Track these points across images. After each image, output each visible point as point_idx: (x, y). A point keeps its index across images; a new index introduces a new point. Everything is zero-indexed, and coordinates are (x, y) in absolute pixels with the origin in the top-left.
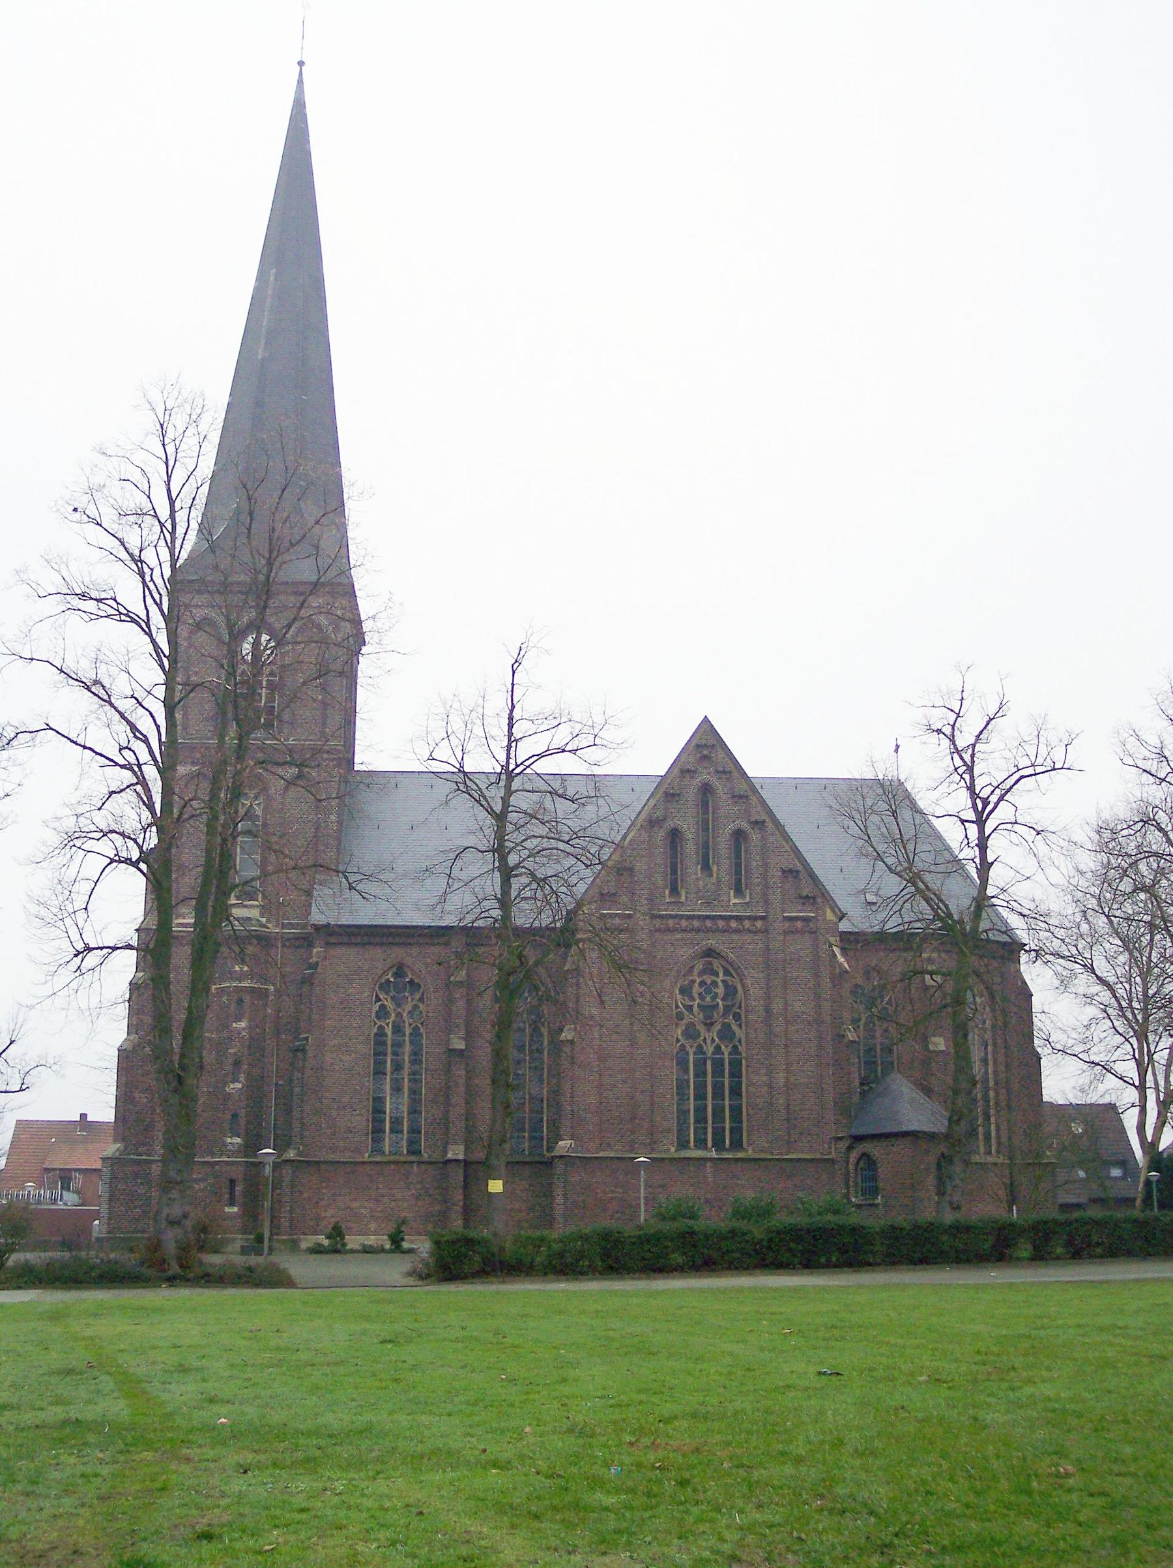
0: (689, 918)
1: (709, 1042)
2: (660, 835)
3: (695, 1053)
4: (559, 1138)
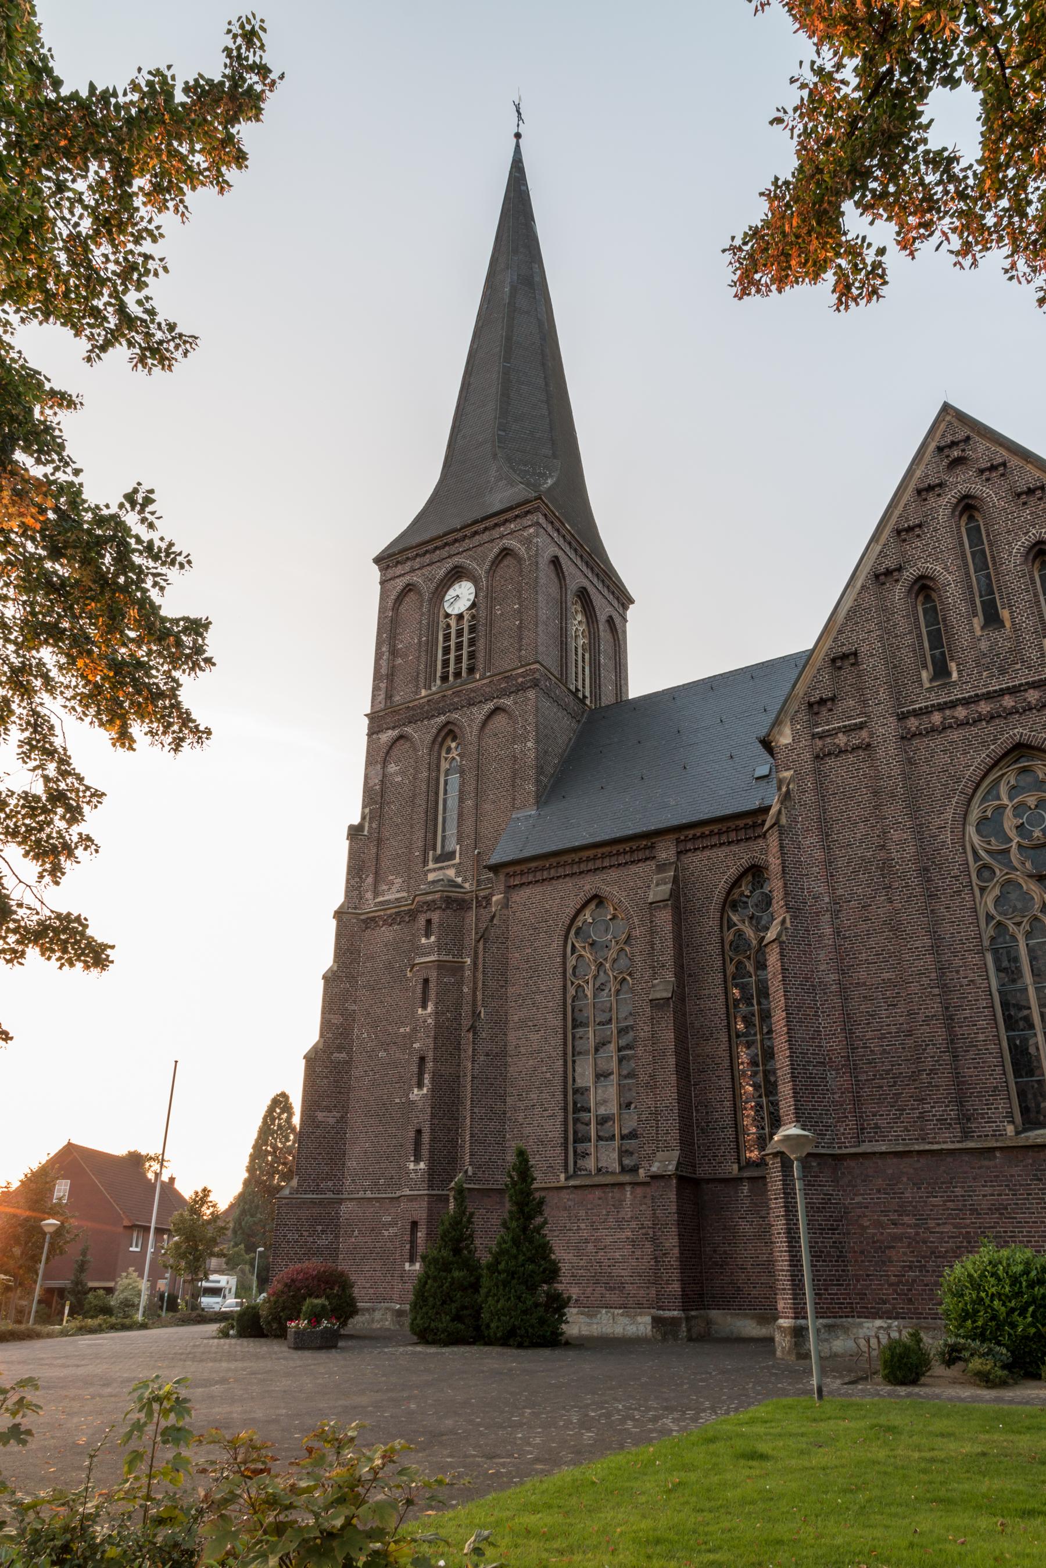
0: (966, 702)
2: (898, 592)
3: (1028, 935)
4: (776, 1123)
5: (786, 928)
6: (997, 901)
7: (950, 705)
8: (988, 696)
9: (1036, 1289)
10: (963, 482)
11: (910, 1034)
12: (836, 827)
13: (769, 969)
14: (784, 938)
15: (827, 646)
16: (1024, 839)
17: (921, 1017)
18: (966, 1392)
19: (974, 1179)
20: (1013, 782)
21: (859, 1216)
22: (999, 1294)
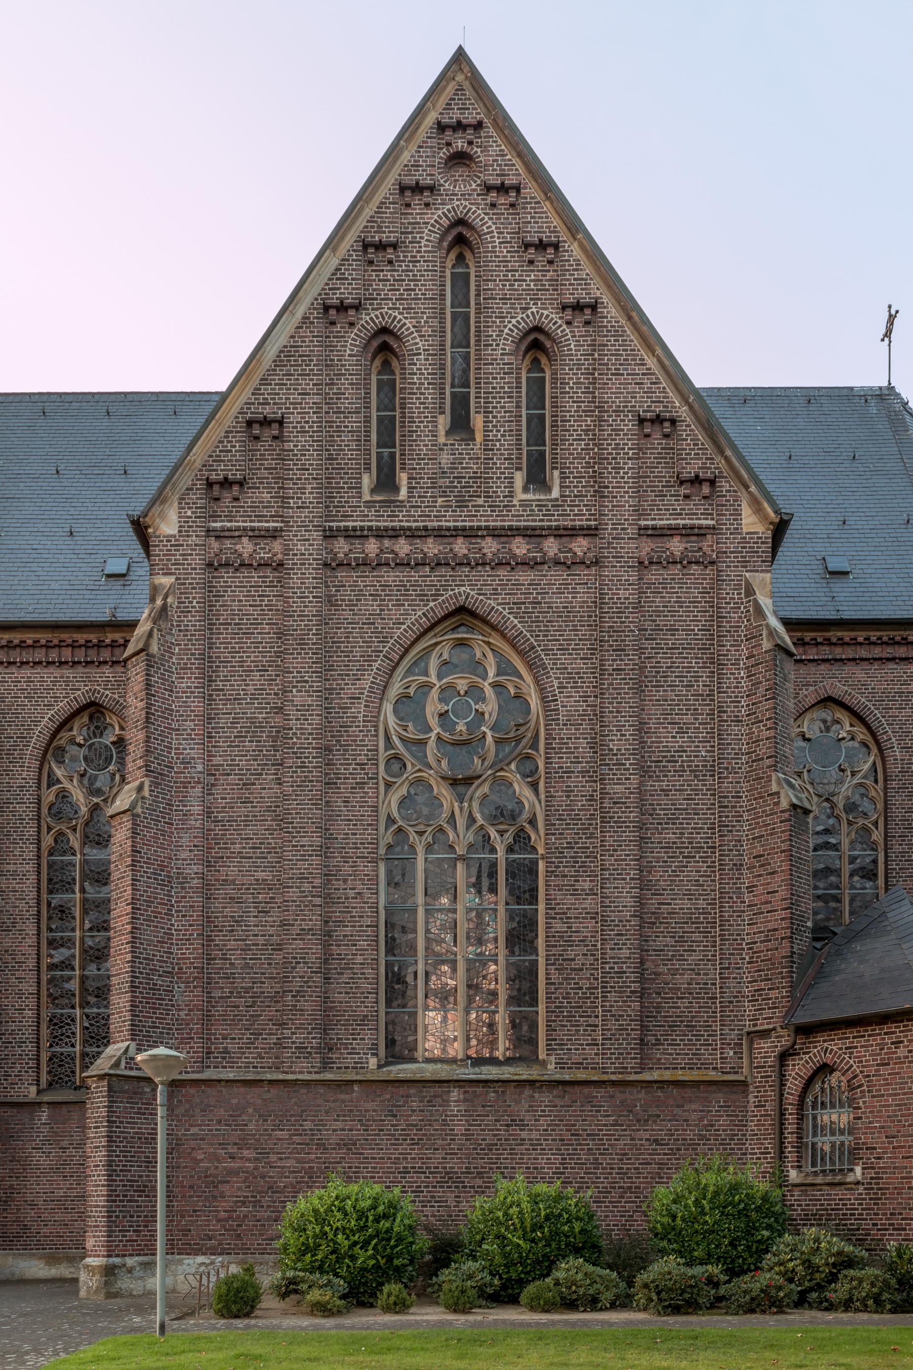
0: (412, 534)
1: (461, 822)
2: (351, 344)
3: (429, 848)
4: (105, 1040)
5: (143, 798)
6: (402, 803)
7: (390, 533)
8: (440, 534)
9: (382, 1223)
10: (460, 196)
11: (279, 948)
12: (223, 672)
13: (114, 848)
14: (139, 810)
15: (243, 399)
16: (445, 731)
17: (295, 930)
18: (306, 1322)
19: (327, 1112)
20: (446, 656)
21: (193, 1149)
22: (344, 1228)
